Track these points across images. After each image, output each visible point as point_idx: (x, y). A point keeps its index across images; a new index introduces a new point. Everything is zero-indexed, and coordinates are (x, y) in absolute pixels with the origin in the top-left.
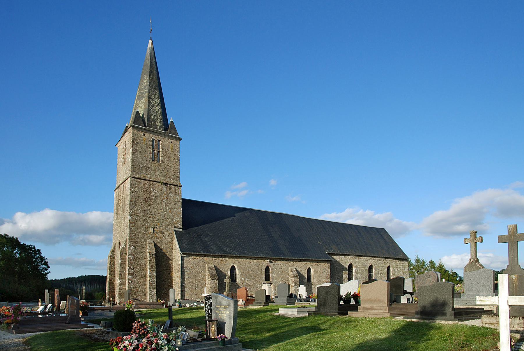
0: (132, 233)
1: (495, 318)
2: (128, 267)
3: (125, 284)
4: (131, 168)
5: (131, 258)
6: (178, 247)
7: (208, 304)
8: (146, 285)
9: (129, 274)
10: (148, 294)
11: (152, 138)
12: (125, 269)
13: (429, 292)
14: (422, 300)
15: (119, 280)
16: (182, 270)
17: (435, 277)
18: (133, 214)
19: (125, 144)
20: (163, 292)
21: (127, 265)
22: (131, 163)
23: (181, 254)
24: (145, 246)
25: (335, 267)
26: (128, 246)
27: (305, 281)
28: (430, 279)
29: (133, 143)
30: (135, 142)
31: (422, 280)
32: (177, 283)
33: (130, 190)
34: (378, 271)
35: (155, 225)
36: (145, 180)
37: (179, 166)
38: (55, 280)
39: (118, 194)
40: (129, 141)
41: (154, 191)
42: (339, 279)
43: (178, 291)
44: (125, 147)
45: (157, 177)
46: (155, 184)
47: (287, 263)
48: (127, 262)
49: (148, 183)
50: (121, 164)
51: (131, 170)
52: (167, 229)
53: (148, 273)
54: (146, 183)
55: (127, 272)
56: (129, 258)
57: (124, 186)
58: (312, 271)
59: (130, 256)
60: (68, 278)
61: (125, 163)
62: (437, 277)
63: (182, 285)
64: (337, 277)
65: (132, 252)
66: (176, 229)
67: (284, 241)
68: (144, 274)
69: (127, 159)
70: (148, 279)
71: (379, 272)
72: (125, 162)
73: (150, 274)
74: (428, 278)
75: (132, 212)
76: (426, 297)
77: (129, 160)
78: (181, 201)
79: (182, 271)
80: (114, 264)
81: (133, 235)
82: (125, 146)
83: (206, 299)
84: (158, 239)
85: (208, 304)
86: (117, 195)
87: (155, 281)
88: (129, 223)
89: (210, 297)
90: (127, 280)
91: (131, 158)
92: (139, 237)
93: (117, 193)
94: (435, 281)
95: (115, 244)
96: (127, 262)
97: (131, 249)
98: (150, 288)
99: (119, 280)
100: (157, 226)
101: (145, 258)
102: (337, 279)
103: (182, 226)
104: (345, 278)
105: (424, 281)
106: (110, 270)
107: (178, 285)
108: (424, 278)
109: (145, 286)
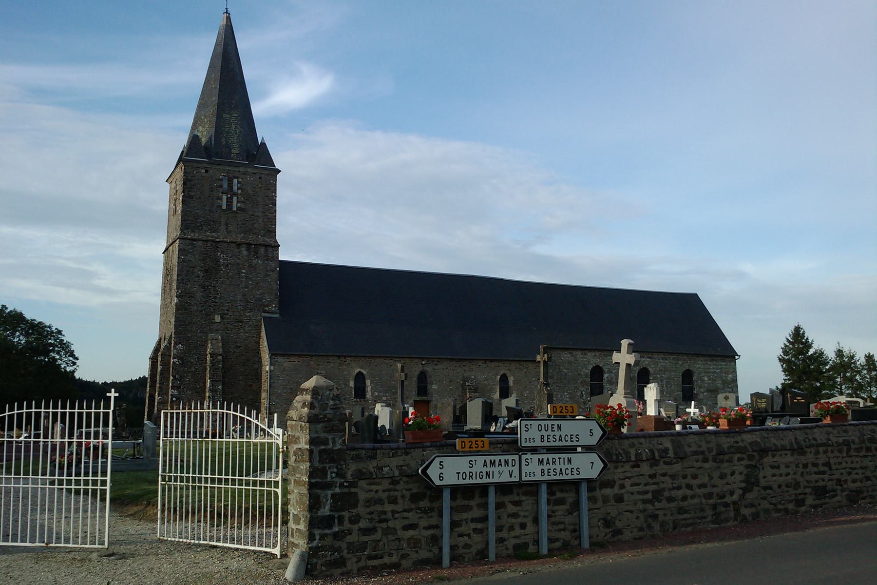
2: (171, 377)
5: (177, 363)
6: (266, 343)
9: (173, 387)
11: (222, 174)
16: (270, 380)
24: (205, 343)
25: (563, 373)
27: (494, 398)
29: (185, 186)
30: (189, 185)
33: (178, 258)
35: (224, 310)
36: (207, 241)
38: (111, 383)
41: (223, 256)
42: (570, 393)
45: (230, 234)
46: (226, 246)
47: (459, 366)
48: (171, 369)
49: (211, 245)
58: (511, 380)
59: (175, 360)
60: (136, 379)
63: (269, 404)
64: (567, 391)
65: (178, 353)
66: (267, 315)
68: (200, 387)
75: (180, 291)
79: (270, 382)
81: (183, 328)
84: (230, 332)
92: (194, 329)
96: (171, 369)
97: (177, 349)
100: (227, 310)
101: (204, 362)
102: (566, 394)
103: (279, 309)
104: (584, 392)
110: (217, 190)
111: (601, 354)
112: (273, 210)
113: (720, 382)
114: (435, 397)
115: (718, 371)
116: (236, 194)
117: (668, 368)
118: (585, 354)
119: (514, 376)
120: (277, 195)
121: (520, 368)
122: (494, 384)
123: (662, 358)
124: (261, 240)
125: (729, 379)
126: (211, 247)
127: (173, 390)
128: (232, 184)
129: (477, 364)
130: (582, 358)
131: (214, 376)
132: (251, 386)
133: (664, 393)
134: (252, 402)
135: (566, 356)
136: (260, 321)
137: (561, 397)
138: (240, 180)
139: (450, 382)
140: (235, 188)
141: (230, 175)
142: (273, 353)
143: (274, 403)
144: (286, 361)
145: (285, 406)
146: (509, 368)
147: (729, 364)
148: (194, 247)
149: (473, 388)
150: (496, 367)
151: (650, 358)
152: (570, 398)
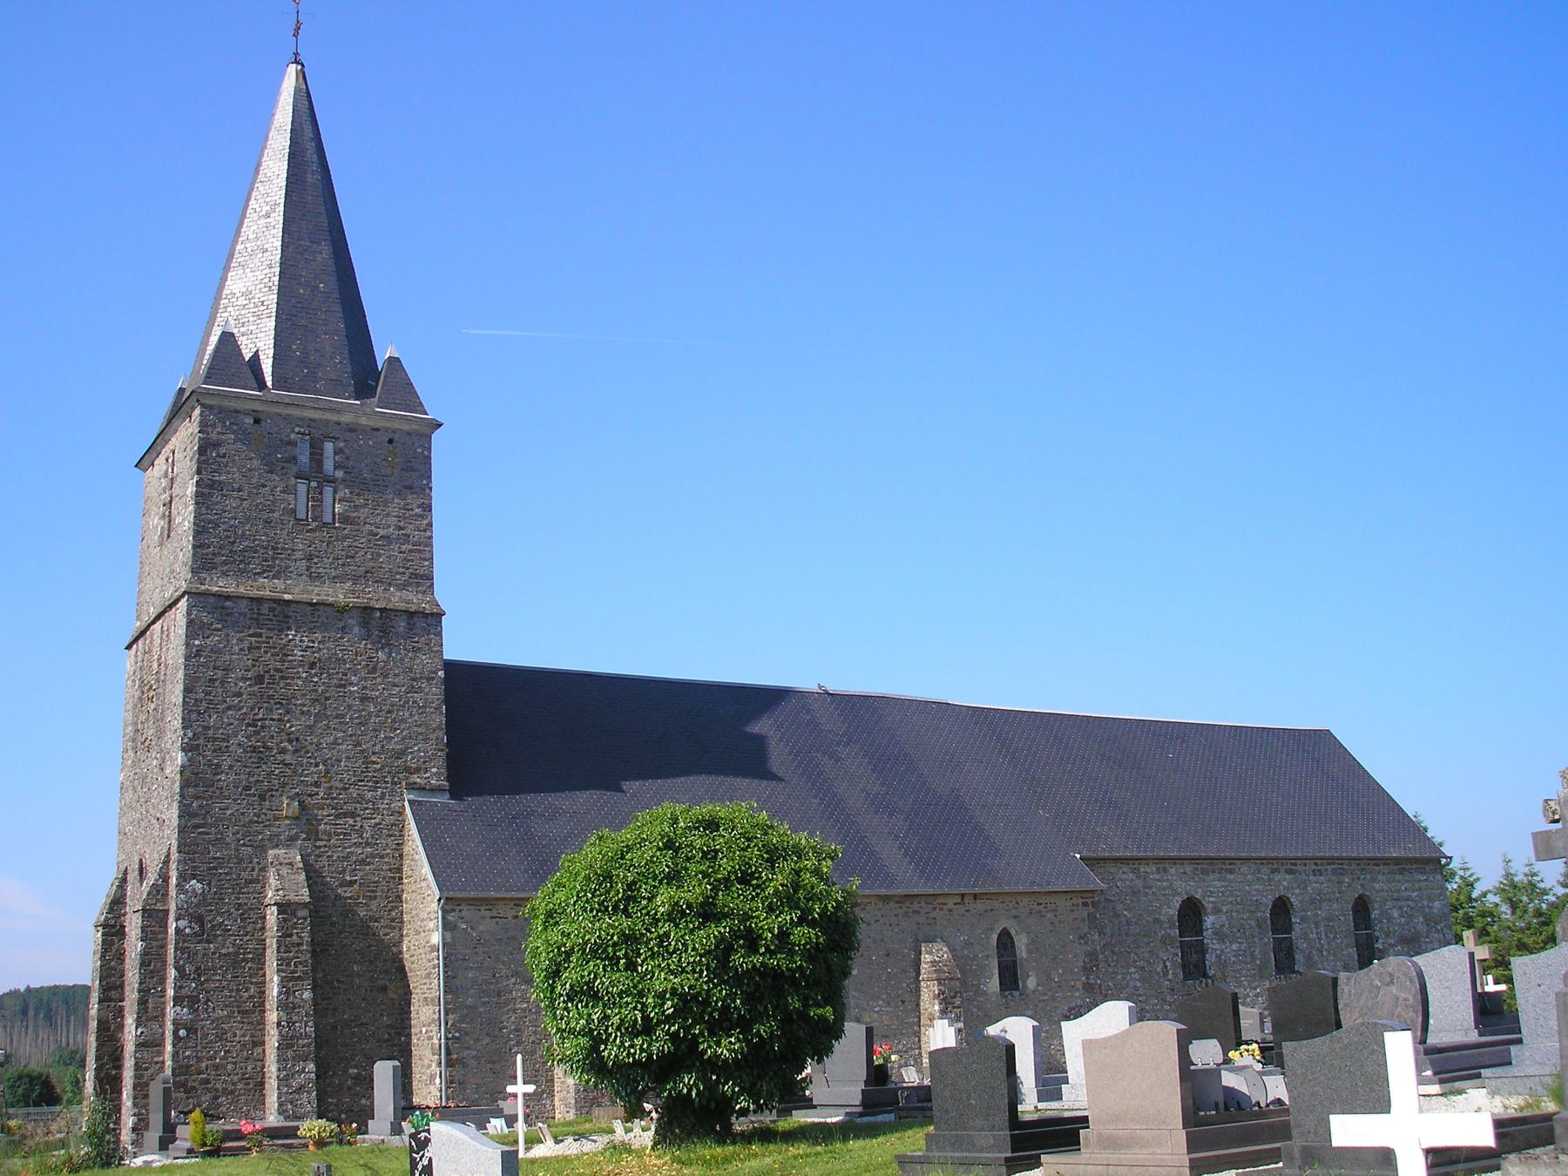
0: (193, 820)
1: (1545, 1163)
3: (160, 1043)
4: (190, 556)
6: (427, 871)
7: (420, 1167)
8: (263, 1043)
9: (178, 1000)
10: (272, 1084)
11: (297, 429)
12: (163, 981)
13: (1324, 1064)
14: (1304, 1101)
15: (137, 1029)
17: (1411, 981)
18: (198, 745)
19: (170, 461)
20: (353, 1071)
21: (171, 959)
22: (191, 538)
23: (439, 900)
26: (173, 881)
28: (1394, 991)
31: (1364, 997)
32: (424, 1030)
33: (187, 644)
34: (1316, 923)
35: (306, 784)
37: (428, 534)
39: (140, 659)
40: (185, 451)
43: (430, 1066)
44: (173, 472)
50: (157, 537)
51: (190, 563)
52: (369, 795)
53: (273, 989)
54: (267, 612)
55: (170, 992)
56: (178, 930)
57: (165, 629)
58: (1021, 943)
59: (182, 923)
61: (169, 536)
62: (1416, 980)
63: (447, 1038)
67: (891, 815)
69: (178, 520)
70: (272, 1016)
71: (1317, 928)
72: (169, 531)
73: (280, 993)
74: (1387, 985)
76: (1314, 1086)
77: (186, 523)
78: (441, 674)
80: (121, 956)
82: (170, 470)
83: (413, 1143)
85: (420, 1167)
86: (136, 663)
87: (310, 1024)
88: (178, 784)
89: (426, 1137)
90: (169, 1026)
91: (193, 515)
93: (136, 656)
94: (1411, 1000)
95: (127, 868)
98: (281, 1059)
99: (134, 1026)
103: (448, 779)
104: (1168, 964)
105: (1372, 999)
106: (100, 980)
107: (430, 1038)
108: (1371, 985)
109: (260, 1050)
110: (283, 468)
111: (1197, 869)
112: (425, 522)
113: (1421, 919)
114: (854, 997)
115: (1415, 894)
116: (331, 481)
117: (1325, 894)
118: (1165, 870)
119: (1028, 933)
120: (434, 485)
121: (1040, 912)
122: (987, 956)
123: (1313, 871)
124: (397, 599)
125: (1435, 911)
126: (271, 617)
127: (178, 1008)
128: (322, 455)
129: (945, 907)
130: (1159, 880)
131: (288, 964)
132: (384, 988)
133: (1324, 952)
134: (389, 1034)
135: (1125, 876)
136: (401, 813)
137: (1124, 979)
138: (342, 444)
139: (888, 955)
140: (328, 465)
141: (317, 433)
142: (451, 894)
143: (457, 1035)
144: (483, 918)
145: (487, 1040)
146: (1014, 912)
147: (1431, 878)
148: (227, 615)
149: (946, 969)
150: (986, 911)
151: (1291, 872)
152: (1142, 979)
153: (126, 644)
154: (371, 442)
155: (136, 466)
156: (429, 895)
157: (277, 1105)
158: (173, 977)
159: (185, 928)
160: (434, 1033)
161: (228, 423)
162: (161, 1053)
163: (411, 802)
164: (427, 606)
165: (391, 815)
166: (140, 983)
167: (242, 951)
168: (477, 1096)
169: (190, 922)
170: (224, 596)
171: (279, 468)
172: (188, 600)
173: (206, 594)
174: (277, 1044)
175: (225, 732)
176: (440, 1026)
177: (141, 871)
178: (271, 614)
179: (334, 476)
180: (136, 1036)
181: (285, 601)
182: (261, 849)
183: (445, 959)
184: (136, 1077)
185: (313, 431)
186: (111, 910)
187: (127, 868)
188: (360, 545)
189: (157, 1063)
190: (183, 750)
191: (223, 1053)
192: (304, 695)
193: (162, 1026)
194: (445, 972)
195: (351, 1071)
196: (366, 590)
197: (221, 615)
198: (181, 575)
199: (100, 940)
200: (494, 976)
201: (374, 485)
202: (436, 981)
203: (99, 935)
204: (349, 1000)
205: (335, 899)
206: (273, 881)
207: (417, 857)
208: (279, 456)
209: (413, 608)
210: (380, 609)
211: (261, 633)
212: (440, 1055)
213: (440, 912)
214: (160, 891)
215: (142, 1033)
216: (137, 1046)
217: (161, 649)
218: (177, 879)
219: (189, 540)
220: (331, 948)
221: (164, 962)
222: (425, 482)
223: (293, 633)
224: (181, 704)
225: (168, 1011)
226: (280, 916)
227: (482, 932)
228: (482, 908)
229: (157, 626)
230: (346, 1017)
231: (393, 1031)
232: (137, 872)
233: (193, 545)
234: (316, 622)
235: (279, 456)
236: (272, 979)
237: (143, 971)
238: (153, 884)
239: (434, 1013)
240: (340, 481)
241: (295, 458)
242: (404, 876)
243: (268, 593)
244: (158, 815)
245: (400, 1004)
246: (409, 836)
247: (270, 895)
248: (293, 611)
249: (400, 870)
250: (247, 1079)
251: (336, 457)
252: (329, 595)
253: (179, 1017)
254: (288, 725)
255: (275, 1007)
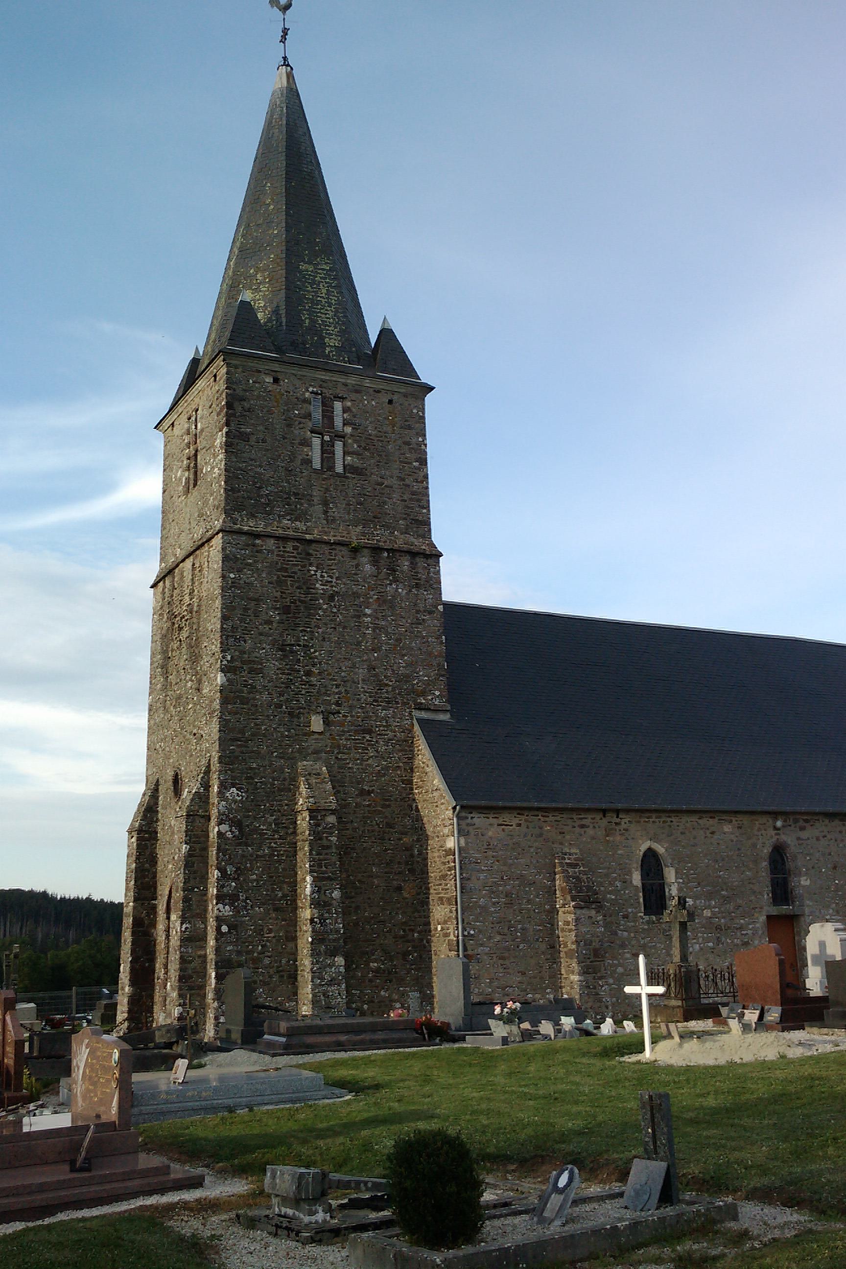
3: (204, 938)
6: (437, 781)
9: (220, 898)
11: (311, 389)
15: (182, 924)
19: (193, 418)
20: (374, 965)
33: (223, 577)
39: (167, 595)
44: (196, 428)
55: (213, 891)
57: (197, 565)
59: (224, 828)
63: (463, 935)
70: (306, 914)
73: (313, 892)
90: (212, 923)
91: (223, 463)
95: (158, 780)
98: (315, 953)
99: (179, 922)
110: (300, 423)
116: (341, 436)
120: (428, 442)
124: (401, 541)
127: (220, 906)
131: (320, 866)
132: (399, 889)
134: (404, 931)
136: (411, 731)
140: (338, 422)
142: (465, 802)
143: (472, 932)
148: (257, 552)
153: (152, 583)
154: (373, 403)
155: (155, 428)
156: (442, 804)
157: (311, 996)
158: (216, 877)
159: (227, 832)
160: (451, 931)
161: (251, 381)
162: (204, 948)
163: (421, 722)
164: (426, 548)
165: (402, 732)
166: (184, 883)
167: (276, 853)
168: (490, 990)
169: (231, 826)
170: (254, 535)
171: (297, 423)
172: (223, 538)
173: (240, 532)
174: (310, 940)
175: (258, 655)
176: (457, 924)
177: (177, 781)
178: (295, 552)
179: (343, 432)
180: (181, 931)
181: (306, 540)
182: (292, 761)
183: (460, 862)
184: (181, 969)
185: (324, 390)
186: (144, 817)
187: (158, 780)
188: (367, 493)
189: (199, 957)
190: (222, 671)
191: (260, 948)
192: (326, 624)
193: (205, 921)
194: (461, 874)
195: (371, 964)
196: (375, 532)
197: (252, 551)
198: (212, 517)
199: (135, 844)
200: (502, 878)
201: (378, 440)
202: (453, 882)
203: (134, 840)
204: (369, 898)
205: (356, 807)
206: (303, 789)
207: (428, 770)
208: (297, 412)
209: (416, 550)
210: (387, 550)
211: (287, 569)
212: (458, 951)
213: (455, 819)
214: (202, 798)
215: (186, 928)
216: (181, 940)
217: (193, 583)
218: (218, 787)
219: (220, 485)
220: (352, 851)
221: (206, 863)
222: (420, 439)
223: (315, 569)
224: (219, 630)
225: (210, 908)
226: (312, 822)
227: (491, 838)
228: (491, 816)
229: (188, 563)
230: (366, 914)
231: (407, 928)
232: (171, 783)
233: (225, 489)
234: (334, 560)
235: (297, 412)
236: (305, 879)
237: (187, 872)
238: (196, 792)
239: (451, 912)
240: (348, 436)
241: (310, 415)
242: (415, 787)
243: (292, 533)
244: (195, 731)
245: (413, 904)
246: (418, 750)
247: (301, 802)
248: (314, 550)
249: (410, 782)
250: (281, 971)
251: (345, 415)
252: (344, 537)
253: (221, 914)
254: (312, 650)
255: (308, 904)
